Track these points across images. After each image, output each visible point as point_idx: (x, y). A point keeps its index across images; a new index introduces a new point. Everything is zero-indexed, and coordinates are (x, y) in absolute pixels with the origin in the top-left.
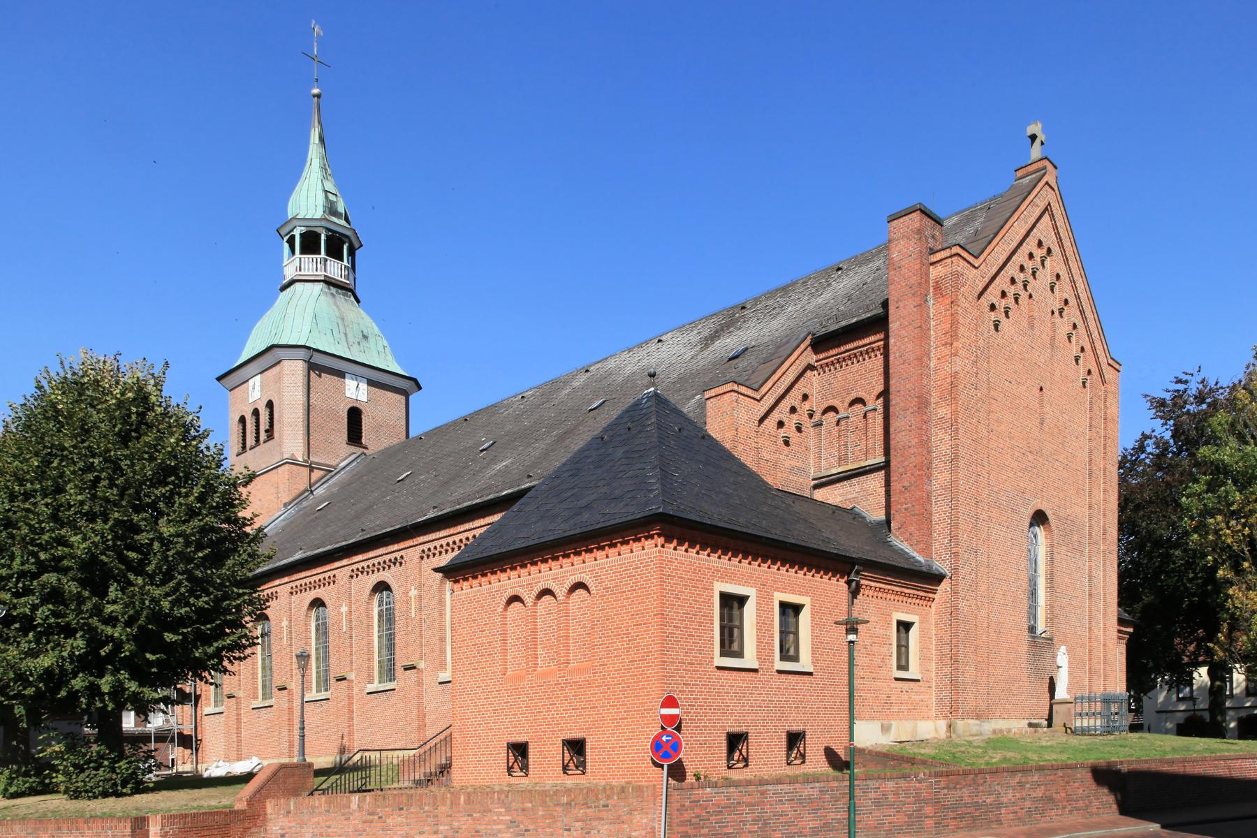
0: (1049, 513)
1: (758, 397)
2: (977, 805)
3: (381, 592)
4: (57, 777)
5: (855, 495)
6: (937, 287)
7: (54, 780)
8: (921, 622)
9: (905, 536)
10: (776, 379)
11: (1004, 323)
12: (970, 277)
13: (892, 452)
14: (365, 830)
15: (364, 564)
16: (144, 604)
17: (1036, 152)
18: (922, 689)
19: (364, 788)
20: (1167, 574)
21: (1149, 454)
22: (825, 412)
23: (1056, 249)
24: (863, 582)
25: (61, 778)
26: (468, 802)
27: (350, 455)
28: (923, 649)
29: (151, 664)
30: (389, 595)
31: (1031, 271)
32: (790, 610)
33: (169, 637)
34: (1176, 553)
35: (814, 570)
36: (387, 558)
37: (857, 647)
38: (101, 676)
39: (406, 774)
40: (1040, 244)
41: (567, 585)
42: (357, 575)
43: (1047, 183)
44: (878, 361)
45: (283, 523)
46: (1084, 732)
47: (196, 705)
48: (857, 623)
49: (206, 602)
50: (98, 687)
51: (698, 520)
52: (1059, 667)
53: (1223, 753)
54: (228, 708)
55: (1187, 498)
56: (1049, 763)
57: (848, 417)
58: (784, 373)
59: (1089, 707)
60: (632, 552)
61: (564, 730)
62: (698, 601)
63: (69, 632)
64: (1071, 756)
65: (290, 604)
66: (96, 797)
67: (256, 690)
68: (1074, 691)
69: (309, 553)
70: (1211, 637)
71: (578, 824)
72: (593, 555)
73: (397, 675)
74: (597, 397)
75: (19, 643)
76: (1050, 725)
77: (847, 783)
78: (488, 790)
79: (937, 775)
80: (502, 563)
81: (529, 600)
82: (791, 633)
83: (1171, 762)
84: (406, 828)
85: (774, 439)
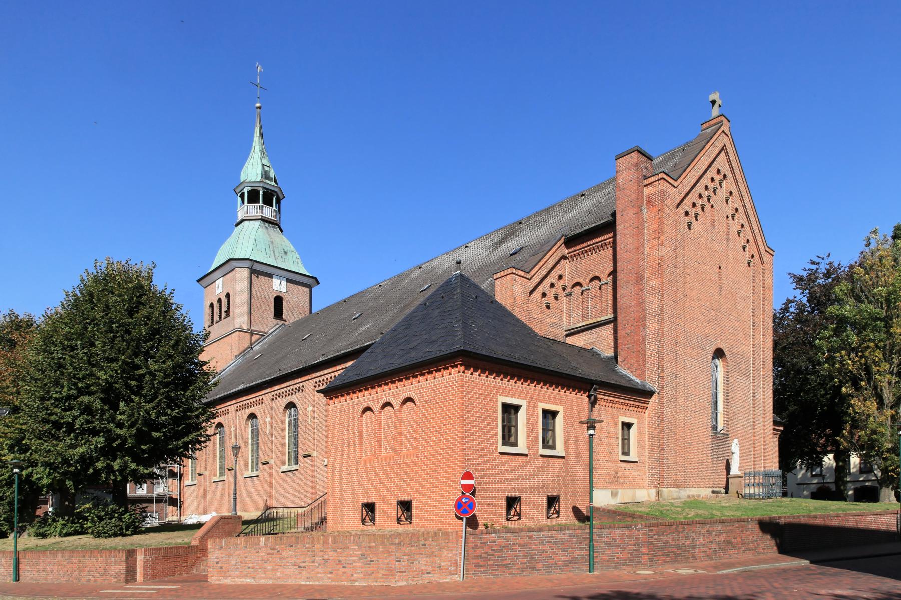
0: (727, 353)
1: (529, 278)
2: (678, 547)
3: (290, 409)
4: (87, 524)
5: (593, 340)
6: (649, 201)
7: (85, 526)
8: (638, 423)
10: (541, 265)
11: (695, 224)
12: (671, 193)
13: (619, 311)
14: (268, 560)
15: (280, 392)
16: (140, 415)
17: (715, 112)
18: (639, 468)
19: (272, 532)
20: (806, 393)
21: (792, 313)
22: (573, 287)
23: (729, 175)
24: (599, 396)
25: (89, 525)
26: (334, 542)
27: (276, 326)
28: (640, 441)
29: (144, 452)
30: (295, 410)
31: (712, 190)
32: (550, 415)
33: (156, 435)
34: (812, 378)
35: (565, 389)
36: (294, 387)
37: (595, 440)
38: (114, 460)
39: (299, 523)
40: (719, 172)
41: (401, 400)
42: (276, 399)
43: (723, 132)
44: (609, 252)
45: (234, 368)
46: (750, 497)
47: (180, 480)
48: (595, 423)
49: (178, 413)
50: (112, 467)
51: (487, 354)
52: (733, 453)
53: (852, 512)
54: (199, 482)
55: (820, 341)
56: (729, 518)
57: (588, 290)
58: (546, 262)
59: (754, 480)
60: (443, 377)
62: (487, 409)
63: (95, 433)
64: (744, 514)
65: (236, 417)
66: (110, 537)
67: (215, 471)
68: (743, 470)
69: (248, 386)
70: (838, 431)
71: (405, 557)
72: (418, 380)
73: (299, 461)
74: (426, 283)
75: (65, 440)
76: (727, 493)
77: (588, 531)
78: (348, 534)
79: (651, 526)
80: (360, 386)
81: (376, 410)
82: (550, 430)
83: (816, 517)
84: (295, 559)
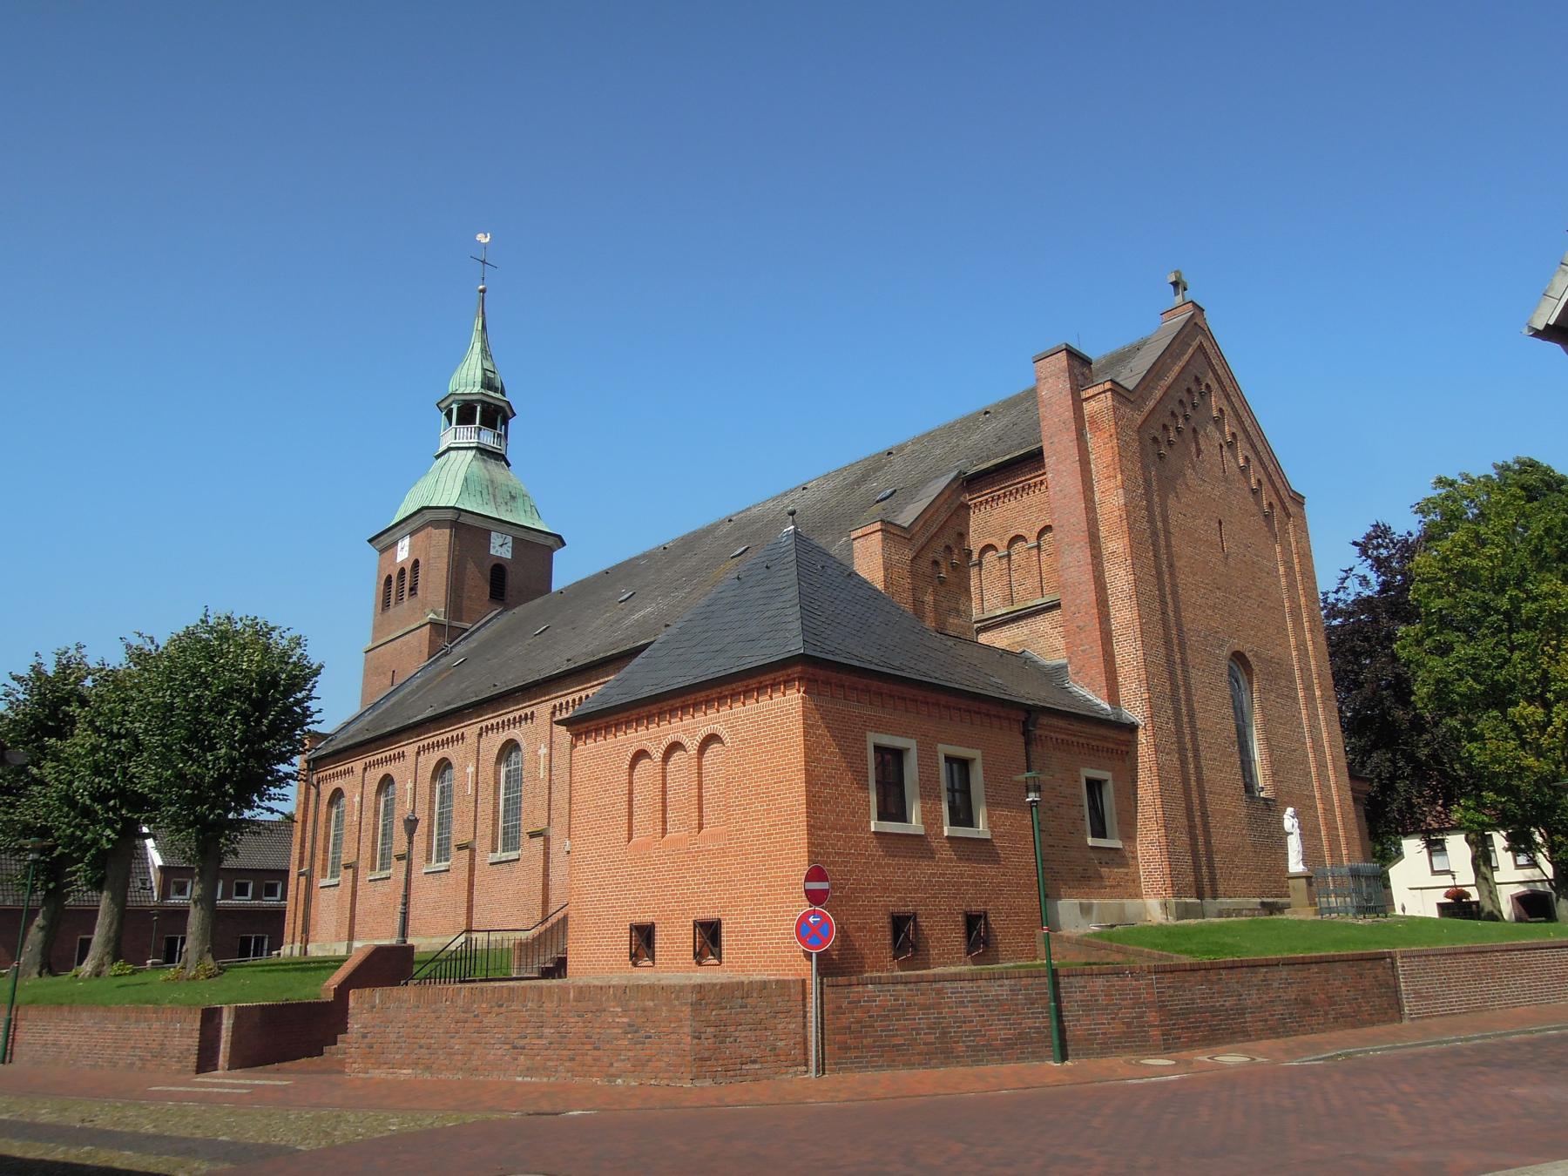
1: (909, 537)
5: (1025, 638)
9: (1087, 681)
61: (696, 909)
85: (929, 579)
